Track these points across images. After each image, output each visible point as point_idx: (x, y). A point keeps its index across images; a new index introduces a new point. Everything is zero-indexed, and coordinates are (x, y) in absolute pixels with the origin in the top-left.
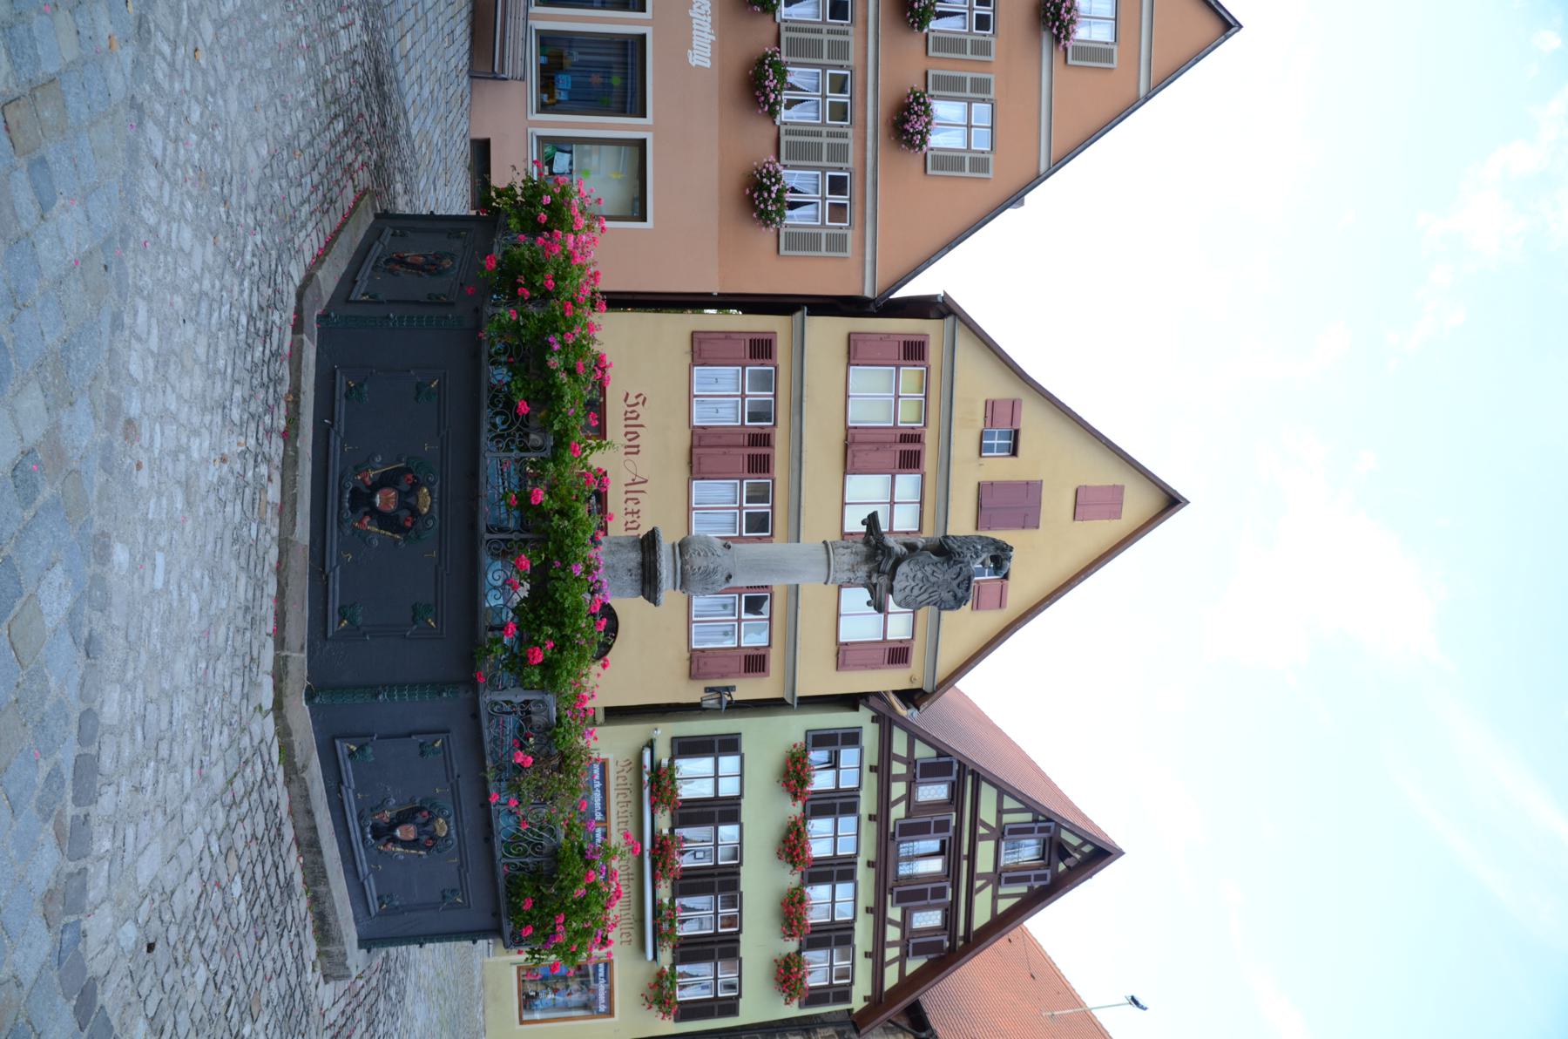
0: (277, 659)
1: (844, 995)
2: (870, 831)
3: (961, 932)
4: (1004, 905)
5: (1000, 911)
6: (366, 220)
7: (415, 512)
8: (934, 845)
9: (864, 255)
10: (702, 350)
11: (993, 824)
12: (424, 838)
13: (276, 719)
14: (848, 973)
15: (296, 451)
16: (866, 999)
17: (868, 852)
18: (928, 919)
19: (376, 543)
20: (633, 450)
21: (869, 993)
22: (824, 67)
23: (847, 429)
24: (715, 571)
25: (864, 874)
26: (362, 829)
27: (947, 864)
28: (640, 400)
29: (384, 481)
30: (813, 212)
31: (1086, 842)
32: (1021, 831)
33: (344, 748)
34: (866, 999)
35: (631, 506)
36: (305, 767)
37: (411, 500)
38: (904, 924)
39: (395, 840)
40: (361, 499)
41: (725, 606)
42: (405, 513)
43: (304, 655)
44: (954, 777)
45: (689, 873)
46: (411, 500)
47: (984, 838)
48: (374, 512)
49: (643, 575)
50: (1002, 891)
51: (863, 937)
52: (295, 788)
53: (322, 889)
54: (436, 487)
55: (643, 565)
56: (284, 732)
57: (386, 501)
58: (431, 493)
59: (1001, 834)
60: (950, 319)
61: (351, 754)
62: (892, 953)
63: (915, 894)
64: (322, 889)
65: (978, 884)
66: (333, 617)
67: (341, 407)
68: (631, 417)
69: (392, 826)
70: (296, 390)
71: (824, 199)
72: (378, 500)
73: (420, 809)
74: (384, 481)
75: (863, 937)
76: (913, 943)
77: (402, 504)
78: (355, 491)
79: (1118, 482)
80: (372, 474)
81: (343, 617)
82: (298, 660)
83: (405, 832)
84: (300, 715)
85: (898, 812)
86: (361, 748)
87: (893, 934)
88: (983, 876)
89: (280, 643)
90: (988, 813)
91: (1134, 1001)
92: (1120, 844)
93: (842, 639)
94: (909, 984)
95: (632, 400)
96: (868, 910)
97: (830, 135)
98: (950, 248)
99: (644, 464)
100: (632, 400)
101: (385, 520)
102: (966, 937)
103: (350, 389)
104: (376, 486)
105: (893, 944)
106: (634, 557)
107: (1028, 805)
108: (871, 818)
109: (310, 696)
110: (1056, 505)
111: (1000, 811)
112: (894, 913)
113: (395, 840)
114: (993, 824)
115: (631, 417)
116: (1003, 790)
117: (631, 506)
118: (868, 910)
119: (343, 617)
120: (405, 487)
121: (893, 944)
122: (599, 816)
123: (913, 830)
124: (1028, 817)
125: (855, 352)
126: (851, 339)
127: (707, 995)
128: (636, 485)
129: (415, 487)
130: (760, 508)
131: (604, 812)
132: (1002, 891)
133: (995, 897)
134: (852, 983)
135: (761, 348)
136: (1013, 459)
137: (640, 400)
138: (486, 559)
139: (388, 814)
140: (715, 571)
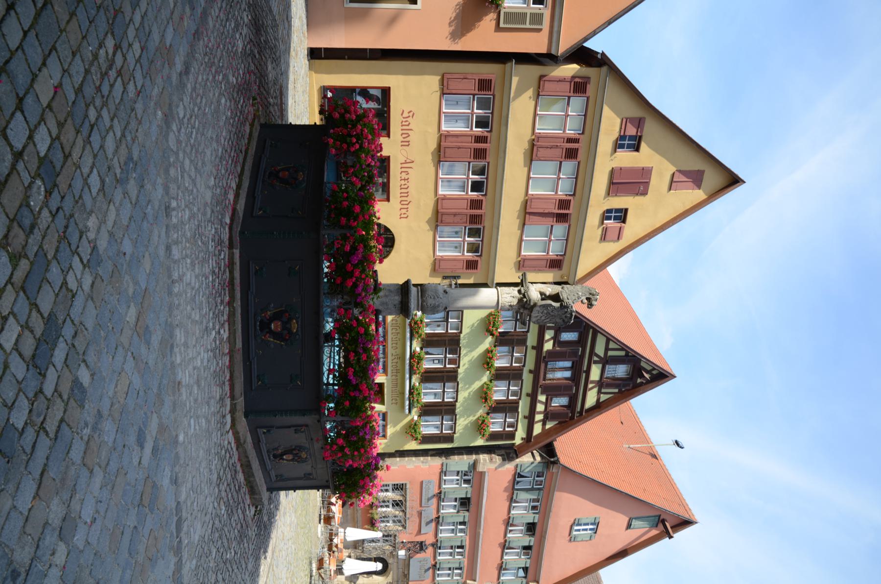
0: (231, 405)
1: (512, 436)
2: (531, 355)
3: (578, 409)
4: (603, 397)
5: (601, 400)
6: (257, 128)
7: (290, 332)
8: (568, 364)
11: (602, 355)
12: (285, 332)
13: (233, 434)
14: (514, 425)
15: (234, 308)
16: (522, 439)
17: (530, 364)
18: (559, 402)
19: (272, 346)
20: (406, 143)
21: (524, 436)
24: (438, 306)
25: (528, 378)
27: (573, 375)
28: (411, 114)
29: (276, 317)
31: (654, 369)
32: (616, 361)
33: (260, 431)
34: (522, 439)
35: (404, 175)
36: (245, 442)
37: (288, 326)
38: (547, 404)
40: (265, 326)
41: (456, 233)
43: (243, 398)
44: (582, 330)
45: (428, 371)
46: (288, 326)
47: (595, 362)
48: (271, 332)
49: (402, 308)
50: (603, 391)
51: (523, 407)
52: (240, 450)
53: (252, 479)
55: (401, 302)
56: (236, 435)
57: (276, 327)
58: (297, 323)
59: (606, 361)
60: (604, 69)
61: (264, 433)
62: (539, 417)
63: (553, 391)
64: (252, 479)
65: (590, 386)
66: (255, 379)
70: (232, 278)
74: (276, 317)
75: (523, 407)
76: (548, 415)
77: (284, 328)
78: (261, 322)
79: (702, 169)
80: (269, 313)
81: (259, 380)
82: (241, 401)
84: (243, 424)
85: (548, 346)
86: (268, 431)
87: (540, 407)
88: (592, 382)
89: (232, 397)
90: (600, 350)
91: (677, 443)
92: (674, 371)
94: (545, 433)
96: (528, 395)
98: (609, 24)
101: (276, 335)
102: (581, 413)
103: (257, 271)
104: (271, 320)
105: (540, 413)
106: (397, 299)
107: (623, 347)
108: (533, 348)
109: (246, 416)
110: (659, 182)
111: (607, 349)
112: (542, 398)
114: (602, 355)
116: (609, 339)
117: (404, 175)
118: (528, 395)
119: (259, 380)
120: (285, 319)
121: (540, 413)
122: (381, 339)
123: (553, 356)
124: (623, 353)
127: (436, 431)
128: (408, 163)
129: (290, 320)
130: (481, 163)
131: (384, 336)
132: (603, 391)
133: (599, 392)
134: (516, 430)
135: (485, 85)
136: (635, 153)
137: (411, 114)
138: (323, 297)
139: (269, 313)
140: (438, 306)
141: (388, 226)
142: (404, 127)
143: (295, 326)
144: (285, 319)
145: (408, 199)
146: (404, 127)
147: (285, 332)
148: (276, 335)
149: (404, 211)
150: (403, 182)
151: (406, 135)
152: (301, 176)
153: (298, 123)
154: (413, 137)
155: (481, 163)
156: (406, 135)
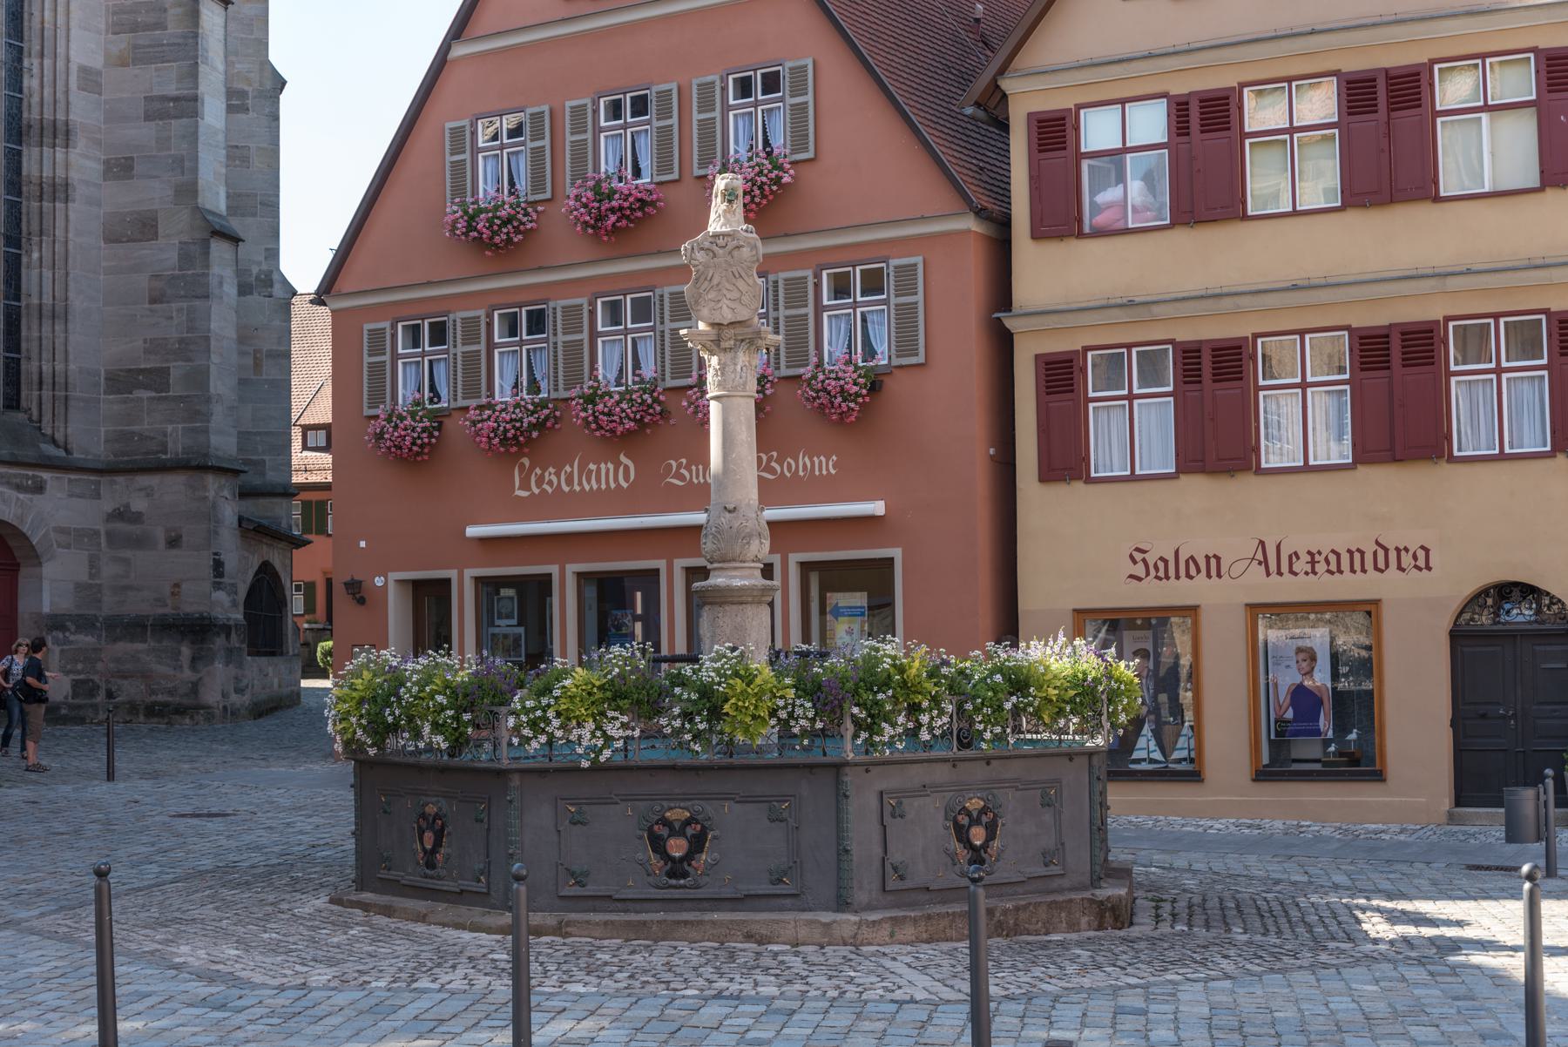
7: (688, 822)
9: (1493, 154)
10: (1066, 461)
12: (984, 819)
20: (1213, 565)
22: (594, 335)
23: (1172, 225)
26: (671, 887)
28: (1138, 556)
30: (442, 364)
35: (1301, 565)
37: (975, 814)
39: (985, 846)
42: (690, 831)
46: (975, 814)
48: (689, 857)
54: (665, 804)
58: (671, 809)
67: (590, 890)
68: (1165, 569)
69: (972, 847)
71: (626, 332)
72: (978, 843)
73: (650, 831)
74: (658, 845)
77: (681, 833)
78: (671, 874)
81: (780, 881)
83: (978, 835)
93: (1533, 180)
95: (1139, 570)
97: (776, 309)
99: (1235, 548)
100: (1139, 570)
101: (697, 844)
113: (985, 846)
115: (1165, 569)
117: (1301, 565)
120: (664, 832)
125: (1062, 218)
126: (1039, 233)
129: (666, 823)
137: (1138, 556)
141: (1469, 589)
142: (1172, 572)
143: (677, 814)
144: (664, 832)
145: (1369, 549)
146: (1172, 572)
147: (984, 819)
148: (991, 835)
149: (1407, 560)
150: (1321, 567)
151: (1189, 567)
152: (431, 809)
153: (350, 816)
154: (1198, 547)
155: (1499, 338)
156: (1189, 567)
